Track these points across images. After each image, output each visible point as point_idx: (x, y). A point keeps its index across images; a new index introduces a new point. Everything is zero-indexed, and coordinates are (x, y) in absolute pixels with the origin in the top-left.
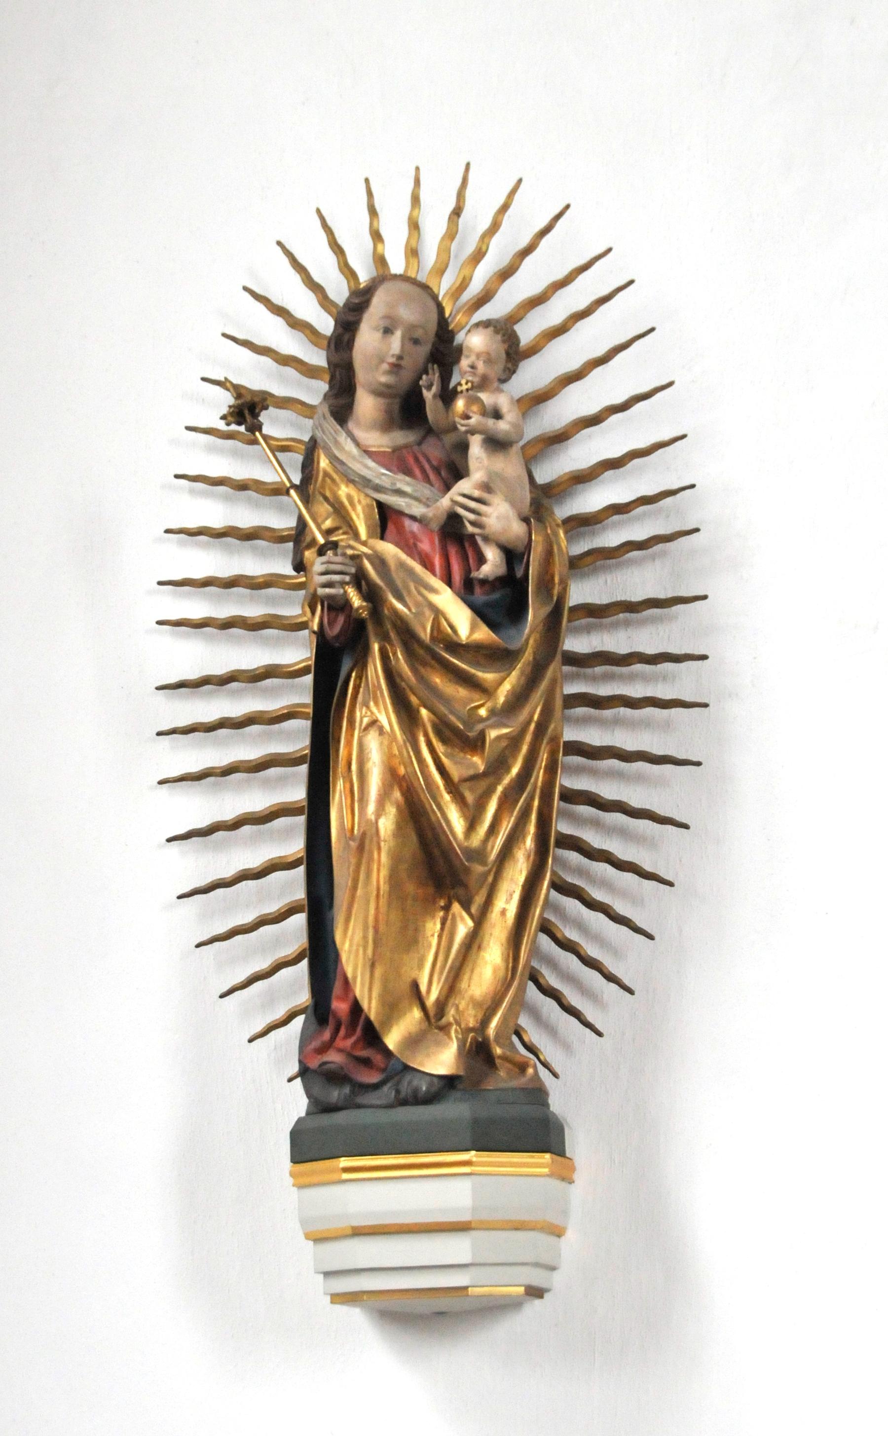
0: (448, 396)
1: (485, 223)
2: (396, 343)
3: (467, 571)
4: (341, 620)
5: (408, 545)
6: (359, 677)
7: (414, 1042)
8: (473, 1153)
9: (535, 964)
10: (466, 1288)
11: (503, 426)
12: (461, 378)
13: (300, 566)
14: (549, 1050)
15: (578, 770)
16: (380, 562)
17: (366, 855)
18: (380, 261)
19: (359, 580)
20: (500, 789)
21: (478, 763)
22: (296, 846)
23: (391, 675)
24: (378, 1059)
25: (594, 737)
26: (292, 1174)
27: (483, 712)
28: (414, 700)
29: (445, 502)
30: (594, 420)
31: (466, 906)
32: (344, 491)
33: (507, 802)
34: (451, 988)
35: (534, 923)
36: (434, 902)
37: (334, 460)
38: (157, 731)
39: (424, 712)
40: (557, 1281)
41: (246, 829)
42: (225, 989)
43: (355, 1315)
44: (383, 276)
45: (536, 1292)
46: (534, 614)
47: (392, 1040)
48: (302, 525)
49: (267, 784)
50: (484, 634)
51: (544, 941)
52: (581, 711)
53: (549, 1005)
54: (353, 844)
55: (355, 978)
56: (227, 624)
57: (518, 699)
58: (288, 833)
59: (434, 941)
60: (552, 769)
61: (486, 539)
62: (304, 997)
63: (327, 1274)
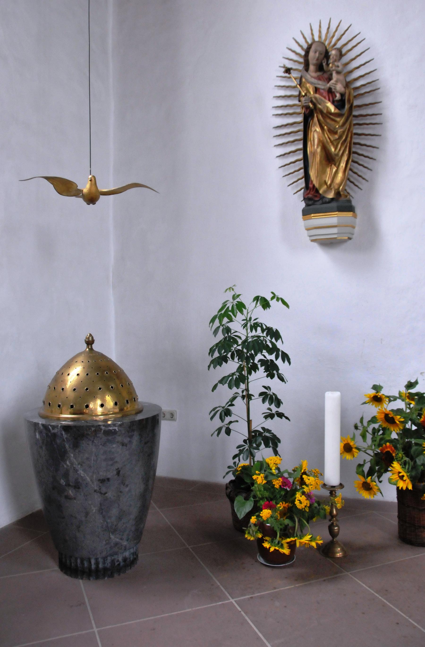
0: (328, 65)
1: (334, 30)
2: (317, 55)
3: (333, 99)
4: (308, 110)
5: (321, 94)
6: (312, 122)
7: (325, 192)
8: (338, 212)
9: (349, 177)
10: (336, 238)
11: (340, 69)
12: (331, 61)
13: (300, 101)
14: (351, 193)
15: (357, 138)
16: (316, 98)
17: (315, 156)
18: (313, 39)
19: (312, 102)
20: (341, 142)
21: (337, 137)
22: (301, 156)
23: (319, 120)
24: (318, 195)
25: (359, 131)
26: (303, 218)
27: (337, 127)
28: (323, 125)
29: (328, 85)
30: (358, 68)
31: (335, 165)
32: (308, 85)
33: (342, 144)
34: (332, 181)
35: (351, 160)
36: (329, 165)
37: (306, 79)
38: (236, 447)
39: (325, 127)
40: (354, 237)
41: (291, 154)
42: (289, 185)
43: (315, 244)
44: (314, 41)
45: (350, 239)
46: (347, 107)
47: (321, 192)
48: (300, 93)
49: (295, 145)
50: (337, 111)
51: (351, 172)
52: (357, 126)
53: (351, 185)
54: (313, 154)
55: (313, 180)
56: (286, 114)
57: (344, 124)
58: (299, 154)
59: (329, 172)
60: (351, 138)
61: (337, 92)
62: (304, 185)
63: (310, 236)
